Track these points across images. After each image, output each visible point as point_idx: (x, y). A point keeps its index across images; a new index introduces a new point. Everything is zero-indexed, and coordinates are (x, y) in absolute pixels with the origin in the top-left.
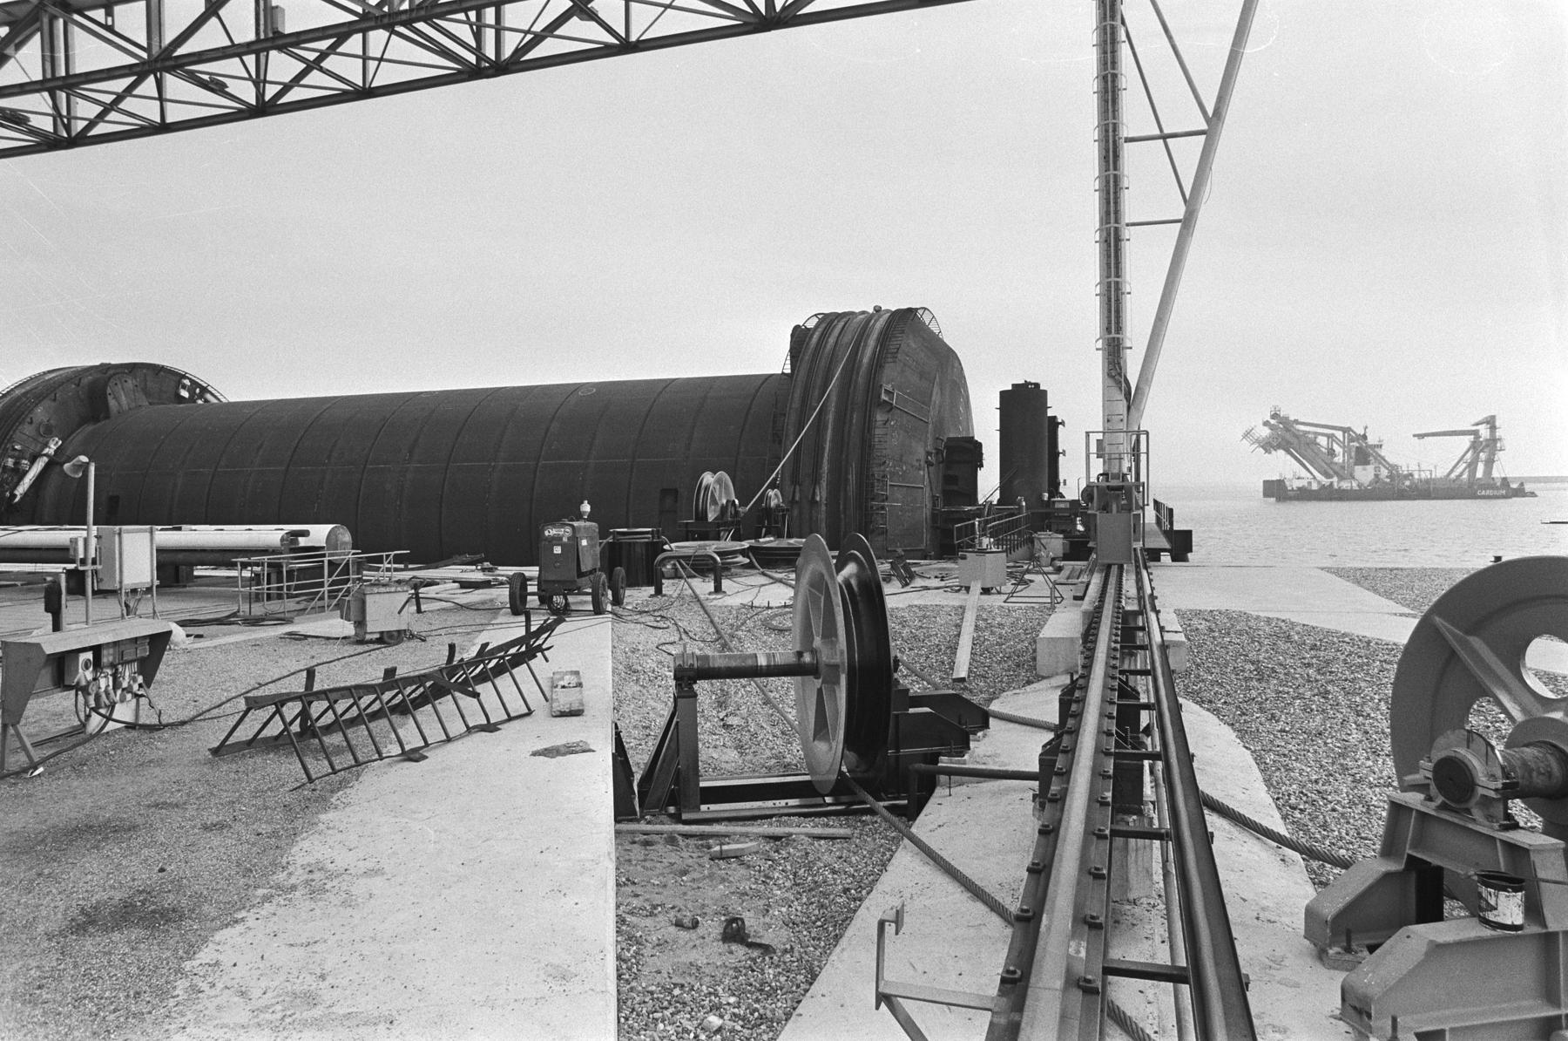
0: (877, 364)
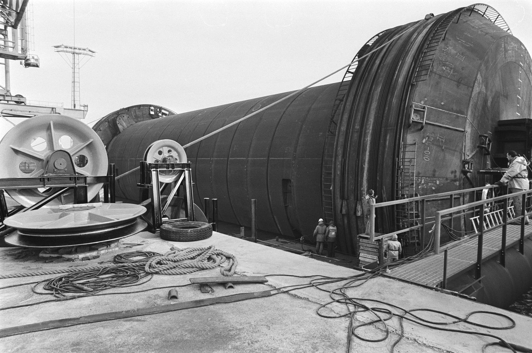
0: (410, 84)
